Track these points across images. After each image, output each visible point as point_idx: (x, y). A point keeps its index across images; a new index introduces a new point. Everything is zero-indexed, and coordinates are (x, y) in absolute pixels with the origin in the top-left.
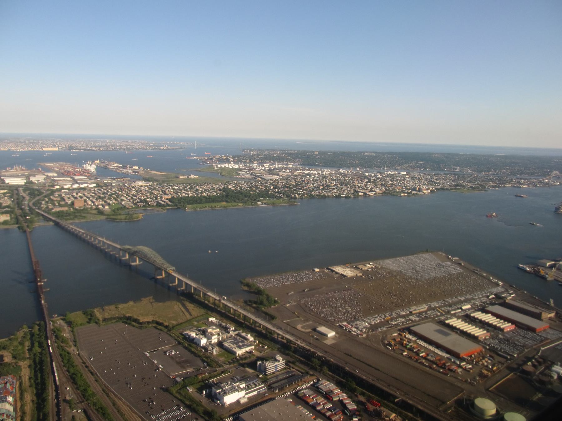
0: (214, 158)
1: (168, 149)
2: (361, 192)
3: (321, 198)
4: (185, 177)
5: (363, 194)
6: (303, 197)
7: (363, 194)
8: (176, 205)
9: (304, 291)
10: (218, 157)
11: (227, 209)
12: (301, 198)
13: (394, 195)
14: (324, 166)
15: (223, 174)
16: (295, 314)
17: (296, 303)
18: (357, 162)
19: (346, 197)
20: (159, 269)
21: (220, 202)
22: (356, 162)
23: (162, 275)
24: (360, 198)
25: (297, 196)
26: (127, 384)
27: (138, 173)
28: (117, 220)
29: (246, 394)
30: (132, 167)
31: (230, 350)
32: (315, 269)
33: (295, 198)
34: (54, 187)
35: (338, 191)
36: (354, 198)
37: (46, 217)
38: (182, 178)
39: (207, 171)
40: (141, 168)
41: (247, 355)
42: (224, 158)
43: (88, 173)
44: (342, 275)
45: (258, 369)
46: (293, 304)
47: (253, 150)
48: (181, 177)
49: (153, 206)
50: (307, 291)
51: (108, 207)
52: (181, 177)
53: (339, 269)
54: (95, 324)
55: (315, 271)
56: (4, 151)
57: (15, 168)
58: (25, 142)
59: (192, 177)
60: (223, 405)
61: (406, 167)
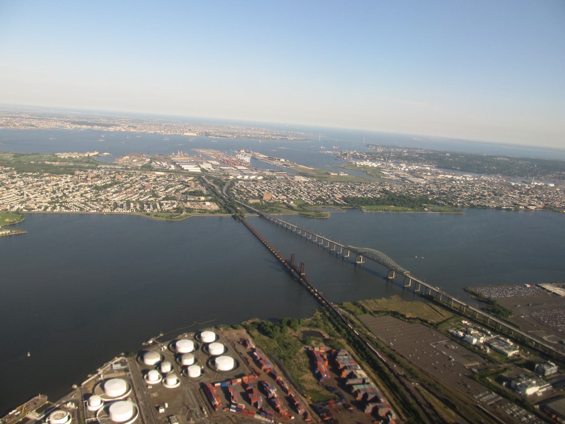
0: (348, 154)
1: (295, 140)
2: (522, 206)
3: (482, 208)
4: (336, 174)
5: (523, 207)
6: (464, 205)
7: (523, 207)
8: (352, 206)
9: (529, 305)
10: (352, 153)
11: (398, 213)
12: (462, 207)
13: (556, 211)
14: (462, 171)
15: (369, 173)
16: (534, 326)
17: (528, 316)
18: (494, 168)
19: (507, 209)
20: (391, 270)
21: (389, 205)
22: (493, 168)
23: (393, 277)
24: (520, 211)
25: (458, 204)
26: (452, 371)
27: (289, 166)
28: (310, 216)
29: (540, 389)
30: (280, 160)
31: (500, 351)
32: (526, 285)
33: (457, 206)
34: (229, 177)
35: (496, 202)
36: (515, 211)
37: (248, 208)
38: (333, 175)
39: (349, 168)
40: (287, 161)
41: (516, 357)
42: (358, 154)
43: (244, 163)
44: (554, 293)
45: (535, 370)
46: (526, 316)
47: (378, 146)
48: (332, 174)
49: (331, 204)
50: (531, 305)
51: (292, 202)
52: (332, 174)
53: (548, 287)
54: (369, 314)
55: (526, 286)
56: (151, 134)
57: (179, 153)
58: (161, 125)
59: (342, 174)
60: (525, 395)
61: (550, 178)
